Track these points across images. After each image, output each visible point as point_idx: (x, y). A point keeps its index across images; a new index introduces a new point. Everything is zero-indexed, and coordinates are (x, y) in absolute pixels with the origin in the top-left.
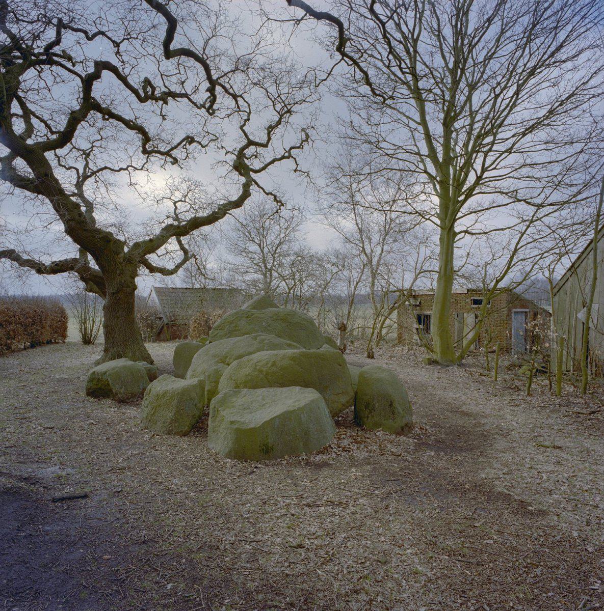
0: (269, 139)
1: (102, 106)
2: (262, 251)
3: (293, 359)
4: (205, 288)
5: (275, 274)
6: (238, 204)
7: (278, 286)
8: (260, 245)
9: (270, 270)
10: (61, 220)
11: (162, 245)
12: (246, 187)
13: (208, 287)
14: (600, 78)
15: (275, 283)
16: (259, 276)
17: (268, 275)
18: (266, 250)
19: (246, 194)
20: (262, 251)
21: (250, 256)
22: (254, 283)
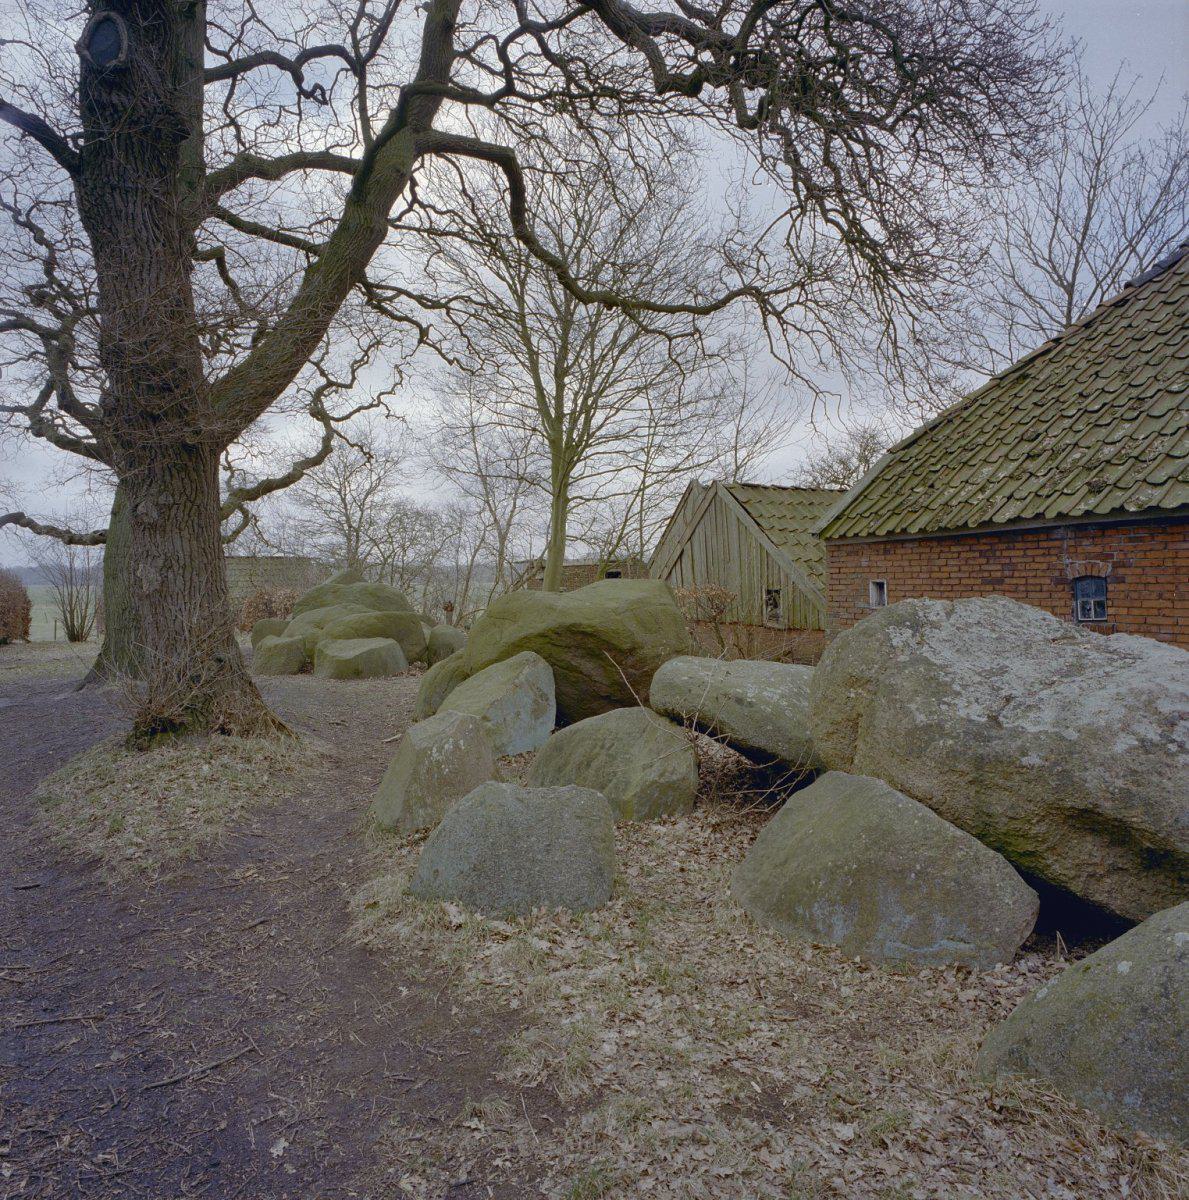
0: (354, 379)
1: (747, 102)
2: (343, 500)
3: (376, 618)
4: (254, 557)
5: (363, 537)
6: (318, 460)
7: (369, 554)
8: (340, 493)
9: (357, 531)
10: (115, 488)
11: (289, 376)
12: (327, 440)
13: (259, 555)
14: (1186, 232)
15: (363, 548)
16: (340, 539)
17: (354, 538)
18: (348, 497)
19: (327, 449)
20: (343, 500)
21: (324, 506)
22: (332, 550)
